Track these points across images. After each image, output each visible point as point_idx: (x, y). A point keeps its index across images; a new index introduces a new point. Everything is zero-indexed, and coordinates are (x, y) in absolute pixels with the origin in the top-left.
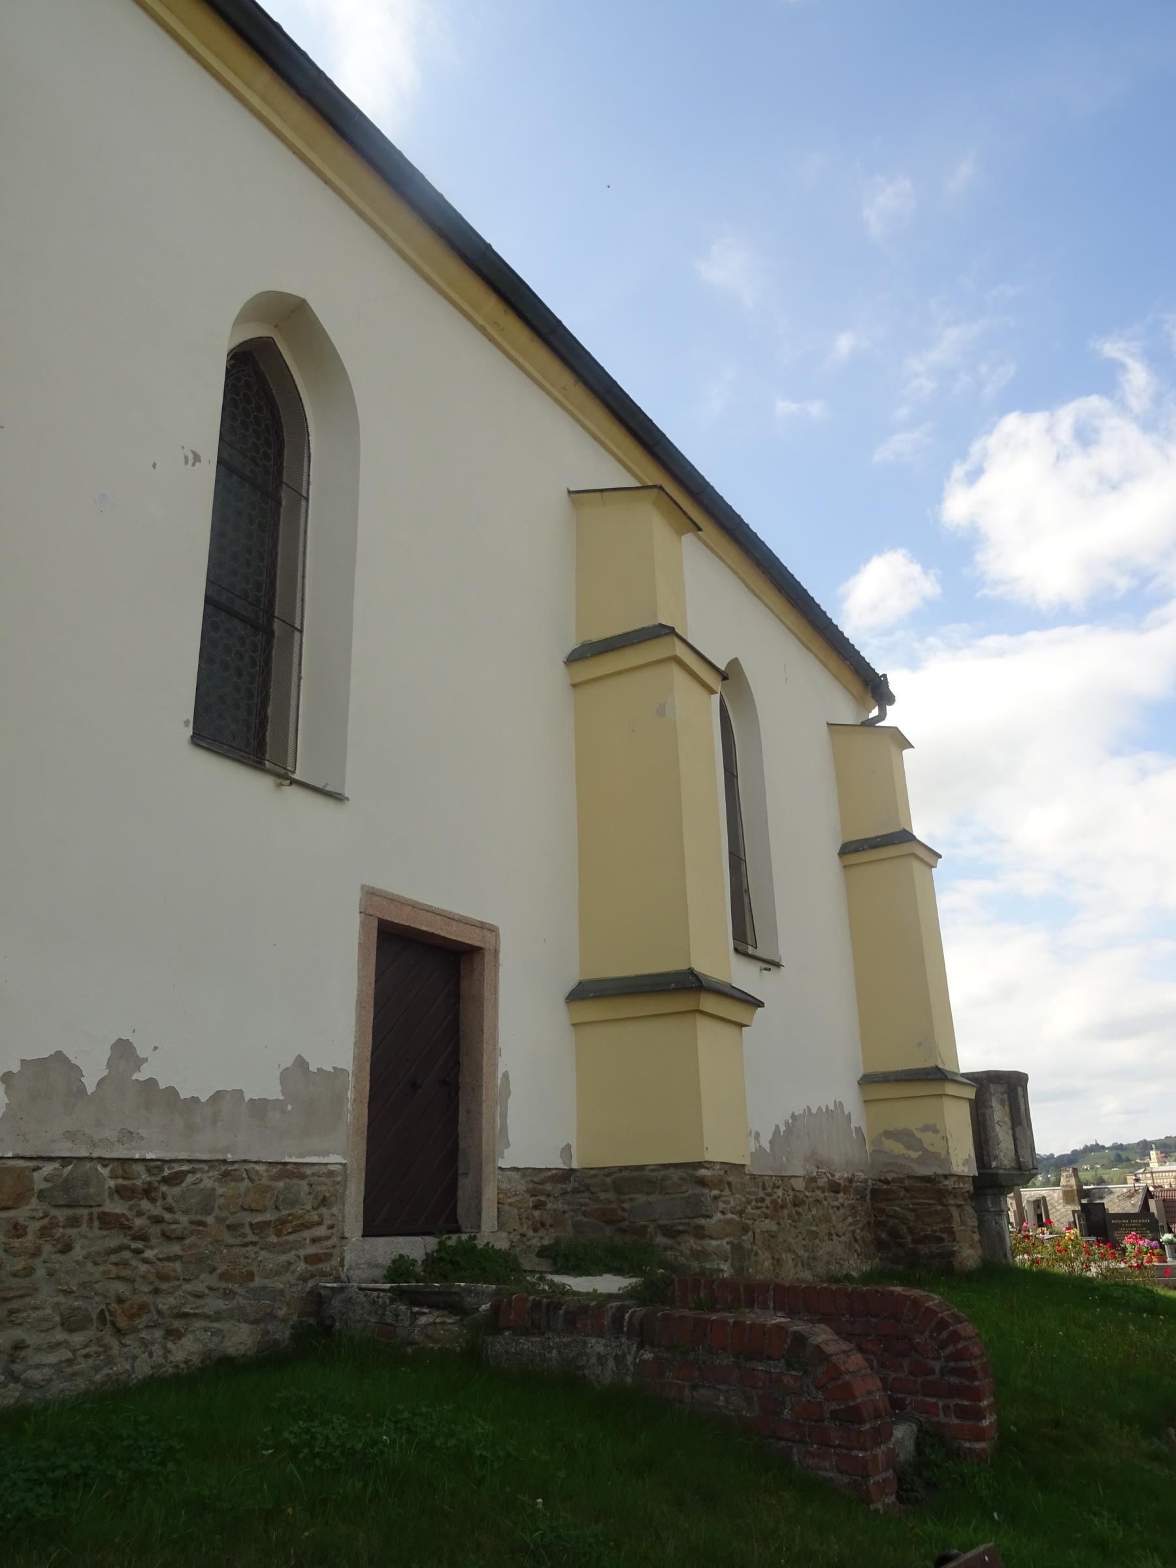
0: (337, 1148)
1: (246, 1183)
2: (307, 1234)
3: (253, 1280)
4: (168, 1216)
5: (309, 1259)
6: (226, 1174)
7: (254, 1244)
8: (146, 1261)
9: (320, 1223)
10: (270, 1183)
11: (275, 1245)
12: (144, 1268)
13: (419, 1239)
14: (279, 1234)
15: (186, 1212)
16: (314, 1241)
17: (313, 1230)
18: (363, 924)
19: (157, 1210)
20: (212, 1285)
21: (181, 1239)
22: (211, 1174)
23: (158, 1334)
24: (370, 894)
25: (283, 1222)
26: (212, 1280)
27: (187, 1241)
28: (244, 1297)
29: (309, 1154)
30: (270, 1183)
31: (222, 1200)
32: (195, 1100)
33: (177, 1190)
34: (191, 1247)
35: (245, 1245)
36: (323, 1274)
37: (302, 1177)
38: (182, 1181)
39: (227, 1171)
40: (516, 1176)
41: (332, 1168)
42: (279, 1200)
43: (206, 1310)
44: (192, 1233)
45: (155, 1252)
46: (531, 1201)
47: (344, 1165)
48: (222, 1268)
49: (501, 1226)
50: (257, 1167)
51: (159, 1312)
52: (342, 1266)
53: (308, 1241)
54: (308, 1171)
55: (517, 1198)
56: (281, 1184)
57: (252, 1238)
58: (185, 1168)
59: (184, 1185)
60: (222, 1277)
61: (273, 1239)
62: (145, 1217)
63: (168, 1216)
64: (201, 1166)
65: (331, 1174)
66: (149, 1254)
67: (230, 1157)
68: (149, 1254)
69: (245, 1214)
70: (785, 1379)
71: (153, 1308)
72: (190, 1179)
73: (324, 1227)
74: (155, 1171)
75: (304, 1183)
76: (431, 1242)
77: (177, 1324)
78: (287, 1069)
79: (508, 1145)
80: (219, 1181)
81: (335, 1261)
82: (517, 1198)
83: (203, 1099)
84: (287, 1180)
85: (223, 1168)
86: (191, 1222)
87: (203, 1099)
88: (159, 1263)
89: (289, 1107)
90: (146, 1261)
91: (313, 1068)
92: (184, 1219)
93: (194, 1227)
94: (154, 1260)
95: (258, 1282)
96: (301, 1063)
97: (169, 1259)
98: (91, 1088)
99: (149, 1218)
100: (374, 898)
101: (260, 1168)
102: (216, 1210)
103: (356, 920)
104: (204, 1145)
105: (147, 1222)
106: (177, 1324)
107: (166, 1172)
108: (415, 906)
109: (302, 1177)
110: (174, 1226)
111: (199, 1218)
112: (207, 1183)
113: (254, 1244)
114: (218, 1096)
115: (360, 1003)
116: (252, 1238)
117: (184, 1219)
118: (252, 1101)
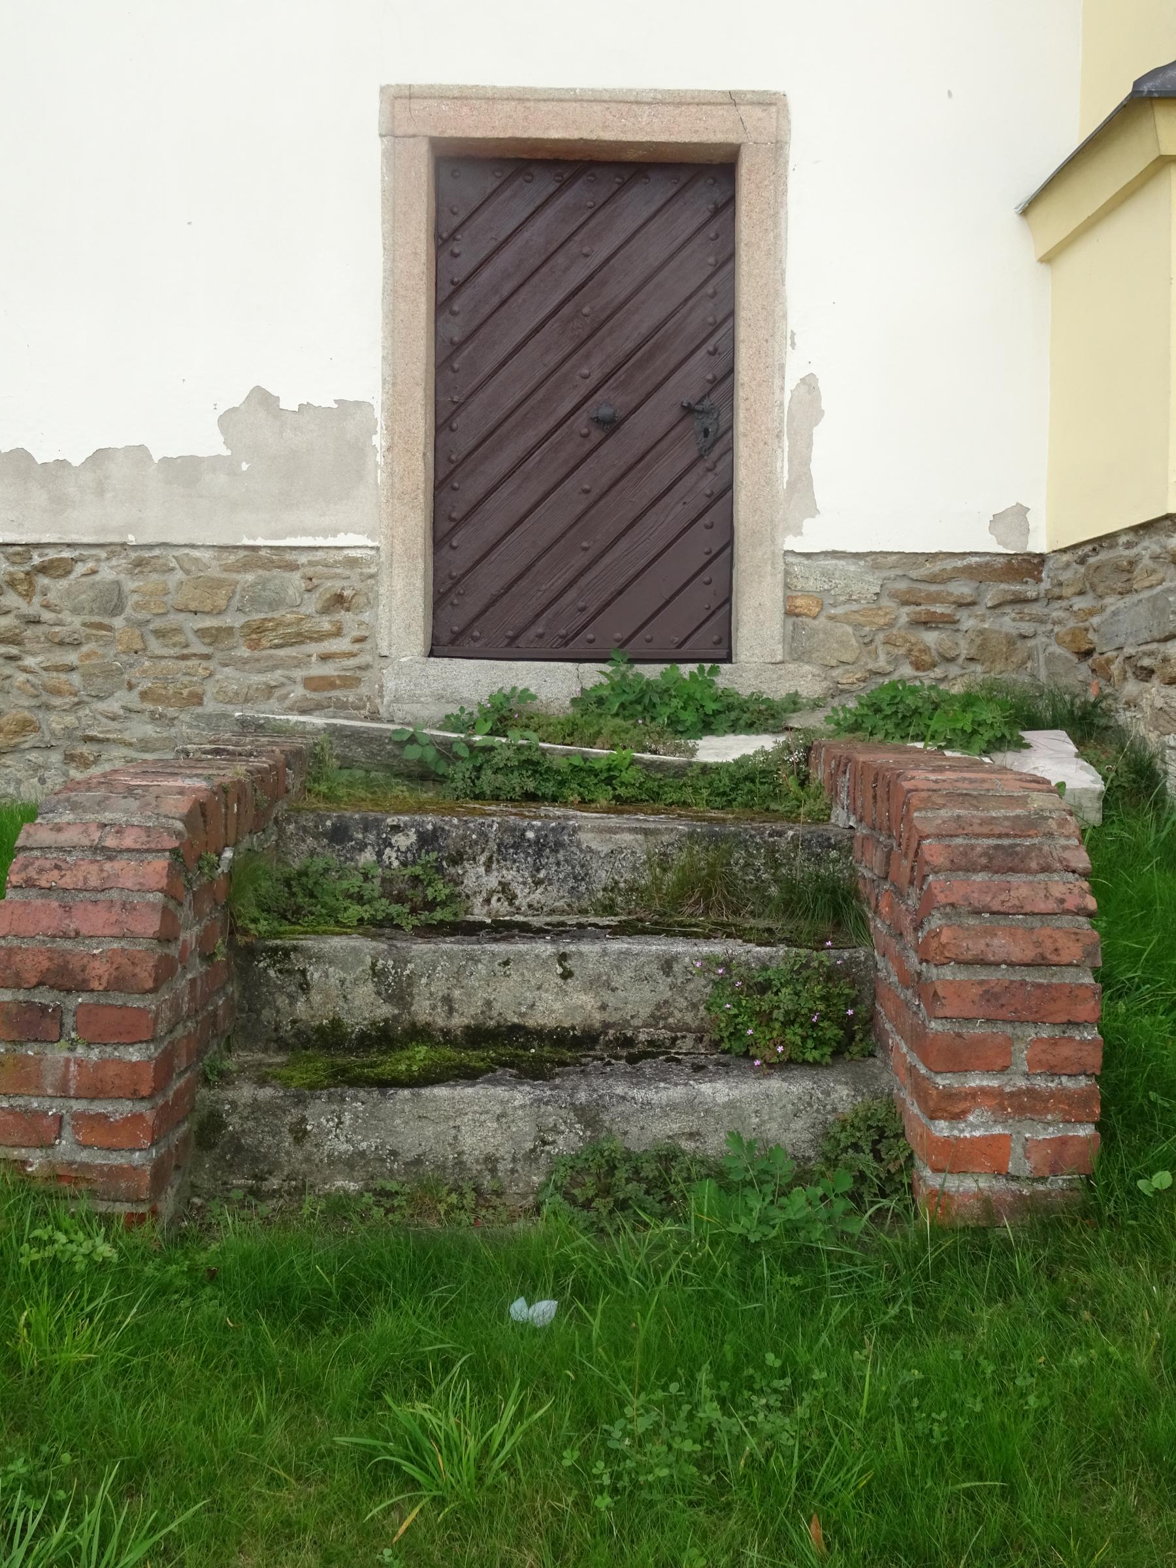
0: (371, 520)
1: (179, 575)
2: (314, 649)
3: (200, 704)
4: (47, 616)
5: (309, 683)
6: (139, 563)
7: (207, 657)
8: (25, 670)
9: (338, 633)
10: (225, 575)
11: (246, 661)
12: (21, 677)
13: (569, 666)
14: (255, 645)
15: (76, 611)
16: (325, 658)
17: (326, 643)
18: (390, 157)
19: (33, 608)
20: (130, 705)
21: (76, 644)
22: (114, 562)
23: (55, 757)
24: (401, 99)
25: (260, 629)
26: (132, 699)
27: (85, 649)
28: (190, 726)
29: (293, 533)
30: (225, 575)
31: (136, 597)
32: (62, 464)
33: (63, 583)
34: (88, 656)
35: (184, 657)
36: (342, 706)
37: (293, 567)
38: (70, 572)
39: (143, 559)
40: (852, 567)
41: (352, 553)
42: (268, 602)
43: (127, 736)
44: (88, 638)
45: (40, 659)
46: (904, 614)
47: (378, 549)
48: (146, 685)
49: (797, 652)
50: (196, 553)
51: (53, 733)
52: (382, 697)
53: (314, 659)
54: (303, 559)
55: (855, 607)
56: (250, 577)
57: (198, 647)
58: (66, 554)
59: (72, 577)
60: (144, 695)
61: (244, 652)
62: (11, 615)
63: (47, 616)
64: (93, 552)
65: (353, 562)
66: (30, 661)
67: (131, 539)
68: (30, 661)
69: (182, 616)
70: (388, 850)
71: (44, 727)
72: (80, 568)
73: (347, 640)
74: (18, 559)
75: (296, 576)
76: (592, 674)
77: (85, 749)
78: (234, 410)
79: (812, 510)
80: (130, 573)
81: (364, 690)
82: (855, 607)
83: (76, 461)
84: (260, 572)
85: (133, 555)
86: (84, 624)
87: (76, 461)
88: (44, 673)
89: (245, 467)
90: (25, 670)
91: (289, 403)
92: (76, 621)
93: (88, 631)
94: (37, 669)
95: (210, 706)
96: (262, 399)
97: (57, 669)
98: (229, 453)
99: (17, 617)
100: (416, 105)
101: (205, 556)
102: (128, 610)
103: (373, 150)
104: (82, 524)
105: (16, 622)
106: (85, 749)
107: (37, 560)
108: (521, 97)
109: (293, 567)
110: (57, 629)
111: (97, 619)
112: (107, 574)
113: (207, 657)
114: (100, 457)
115: (394, 292)
116: (198, 647)
117: (76, 621)
118: (165, 460)
